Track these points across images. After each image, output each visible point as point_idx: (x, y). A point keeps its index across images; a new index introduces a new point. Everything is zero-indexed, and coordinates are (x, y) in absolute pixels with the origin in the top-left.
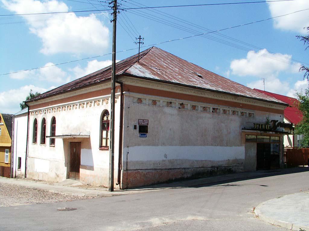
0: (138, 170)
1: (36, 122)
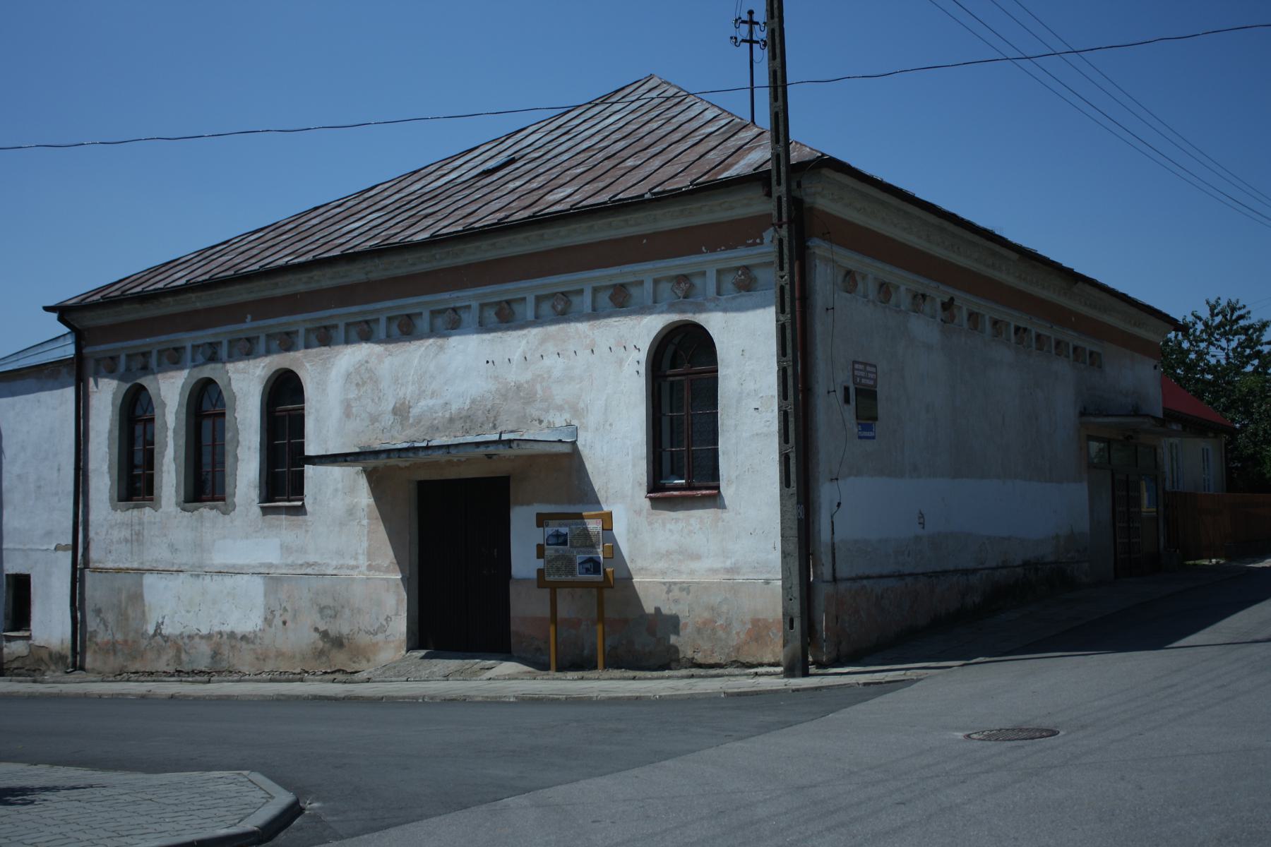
0: (861, 578)
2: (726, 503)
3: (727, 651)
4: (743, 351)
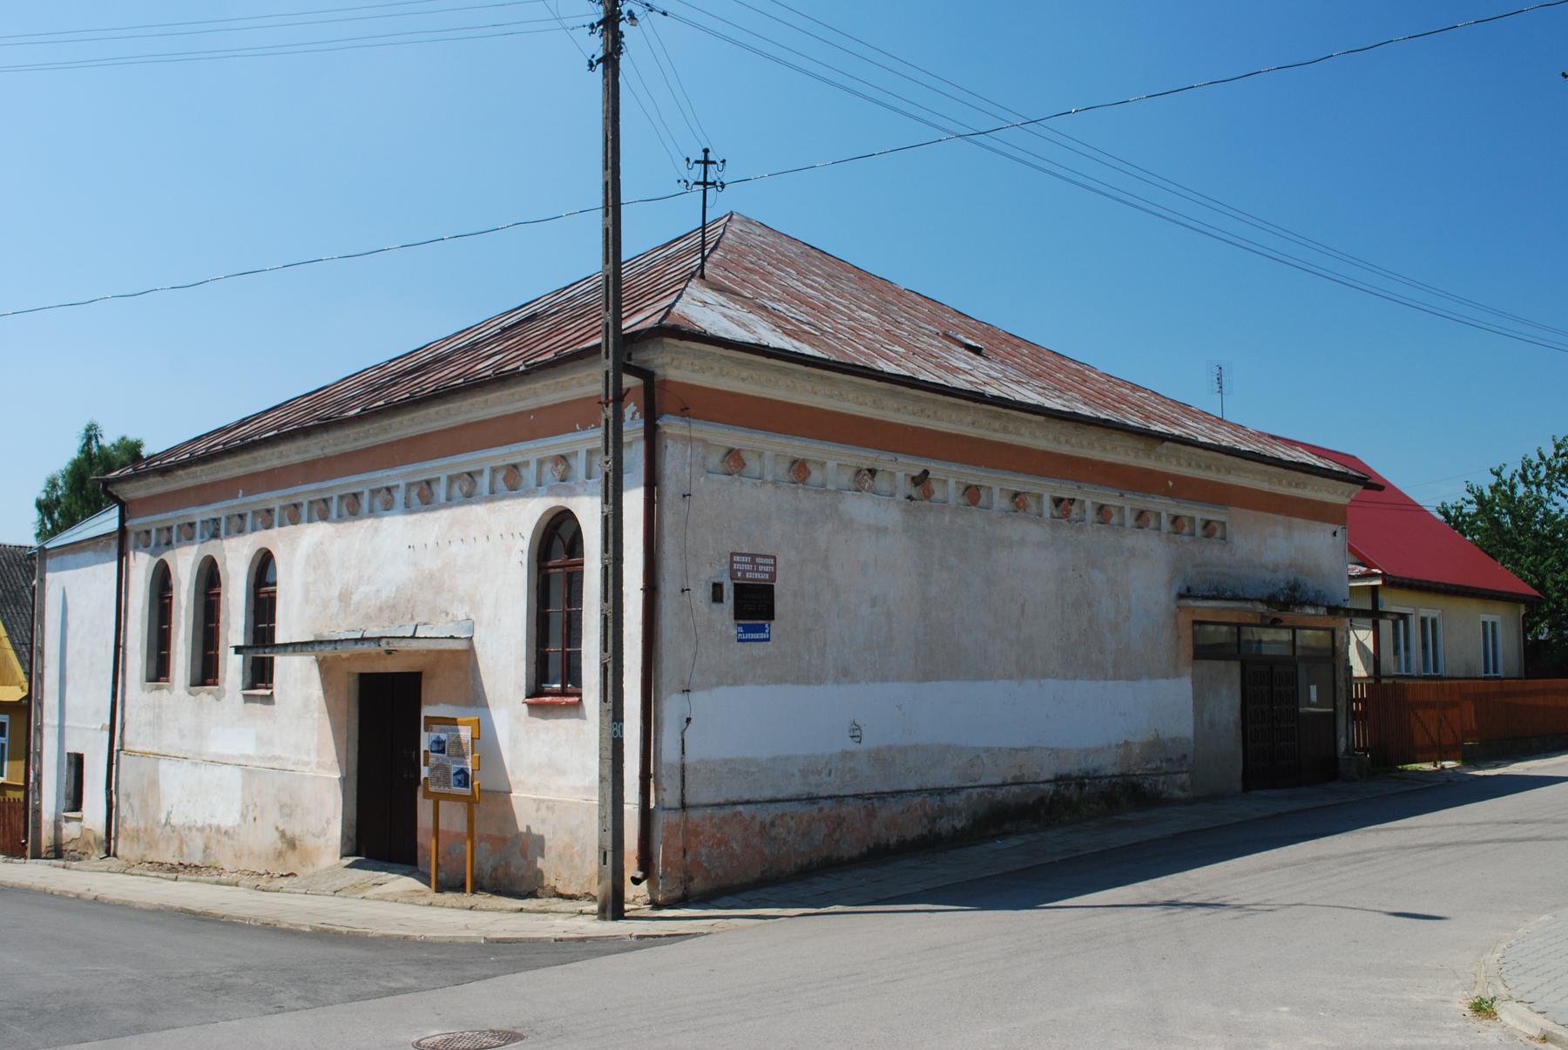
0: (735, 804)
2: (587, 713)
3: (581, 881)
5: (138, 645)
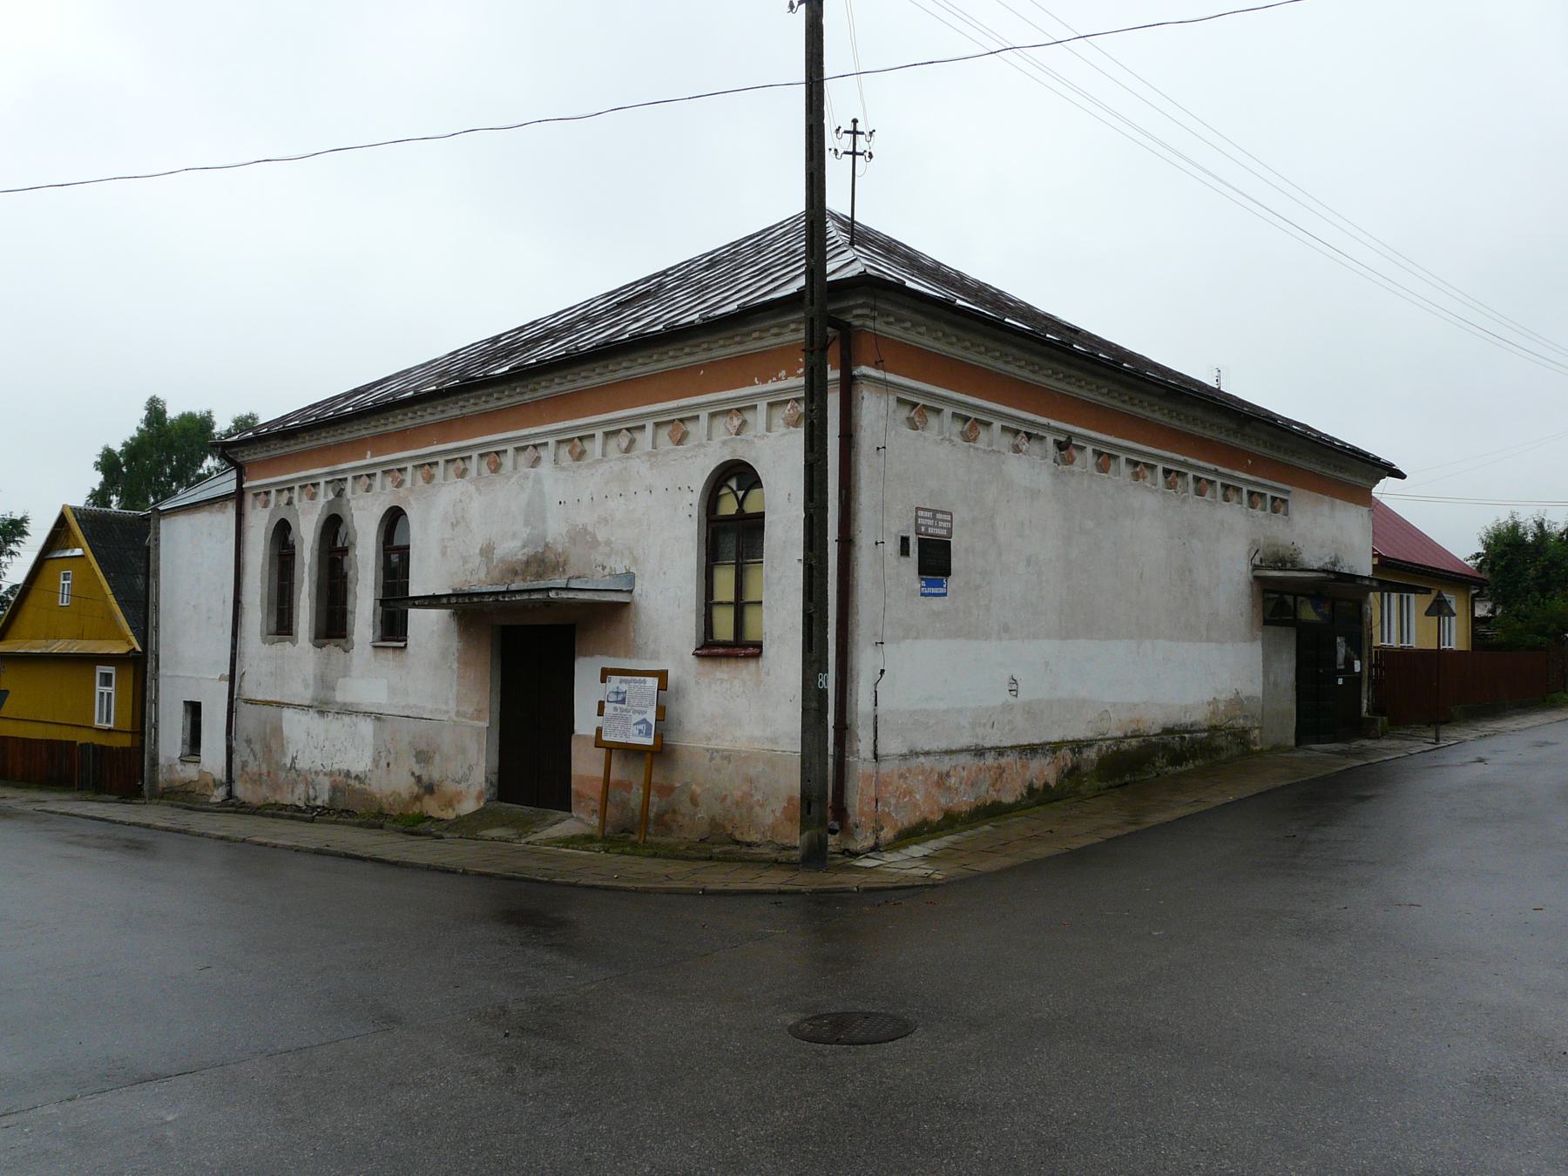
1: (282, 533)
4: (789, 495)
5: (258, 600)
